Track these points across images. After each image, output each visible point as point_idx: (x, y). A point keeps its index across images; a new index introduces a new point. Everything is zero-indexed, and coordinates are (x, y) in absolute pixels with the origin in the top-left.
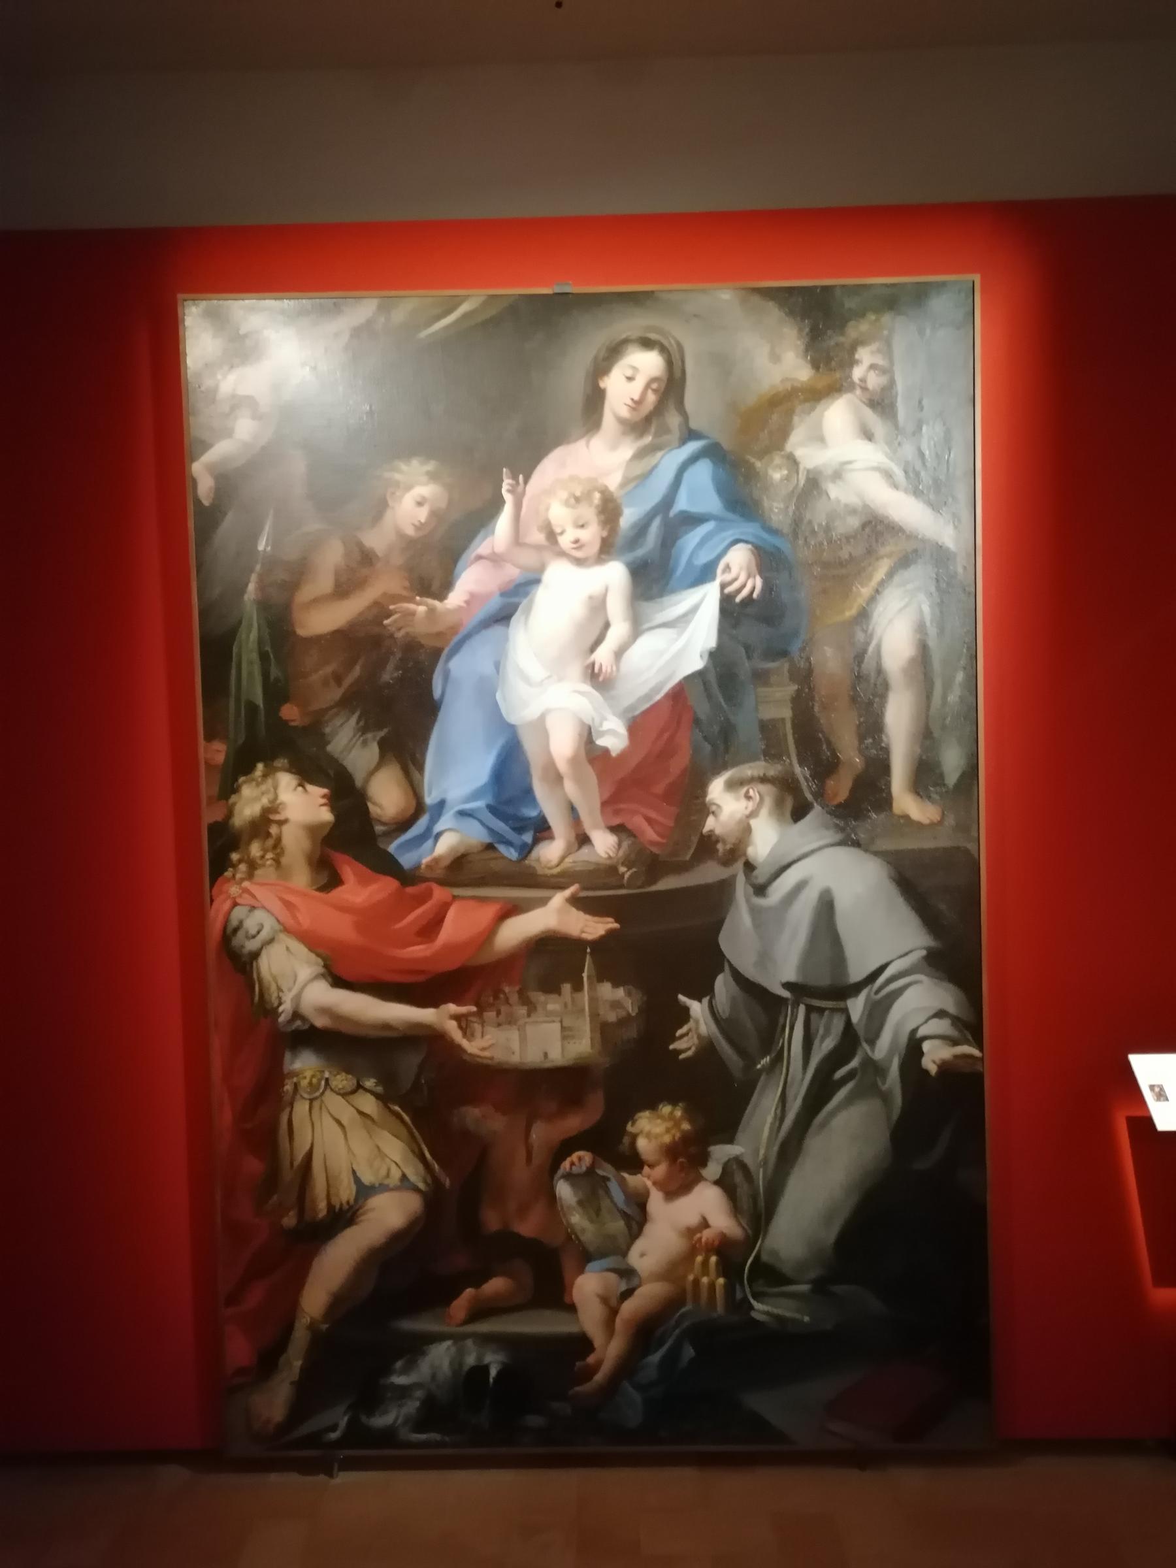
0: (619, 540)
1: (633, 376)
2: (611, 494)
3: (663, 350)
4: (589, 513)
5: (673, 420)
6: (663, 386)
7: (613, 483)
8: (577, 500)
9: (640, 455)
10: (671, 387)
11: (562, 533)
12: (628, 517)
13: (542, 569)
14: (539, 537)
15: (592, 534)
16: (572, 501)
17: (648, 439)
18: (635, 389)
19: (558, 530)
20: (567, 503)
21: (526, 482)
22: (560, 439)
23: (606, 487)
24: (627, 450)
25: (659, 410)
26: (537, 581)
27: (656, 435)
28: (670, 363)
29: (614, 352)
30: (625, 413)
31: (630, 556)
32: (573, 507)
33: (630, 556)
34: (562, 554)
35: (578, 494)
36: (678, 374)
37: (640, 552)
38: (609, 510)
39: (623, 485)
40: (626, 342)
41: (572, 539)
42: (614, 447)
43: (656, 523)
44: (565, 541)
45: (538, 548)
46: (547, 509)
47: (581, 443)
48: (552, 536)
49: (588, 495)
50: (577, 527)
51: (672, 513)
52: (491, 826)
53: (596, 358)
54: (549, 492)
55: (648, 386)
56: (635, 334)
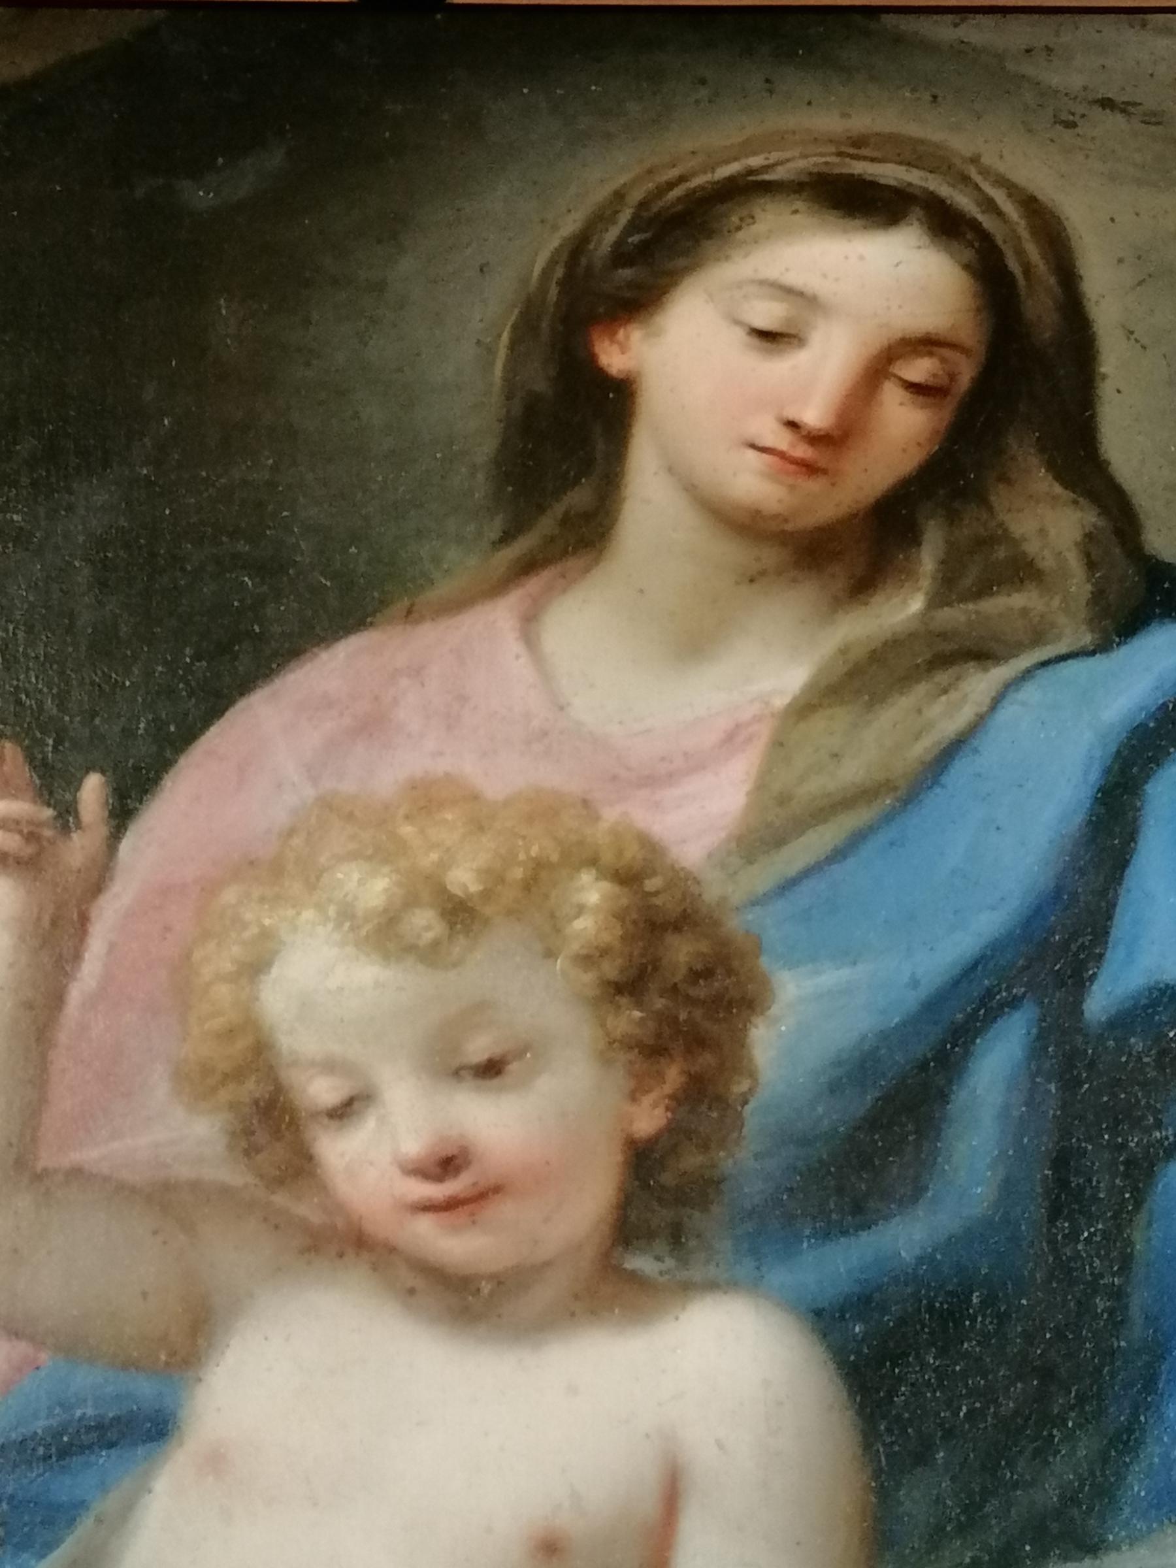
0: (750, 1158)
1: (781, 339)
2: (680, 879)
3: (946, 224)
4: (540, 994)
5: (1048, 522)
6: (966, 373)
7: (698, 820)
8: (460, 914)
9: (861, 681)
10: (1019, 377)
11: (344, 1112)
12: (804, 1025)
13: (190, 1337)
14: (187, 1136)
15: (557, 1119)
16: (424, 923)
17: (902, 608)
18: (815, 381)
19: (323, 1091)
20: (384, 936)
21: (122, 813)
22: (349, 602)
23: (651, 847)
24: (774, 661)
25: (951, 477)
26: (144, 1429)
27: (948, 588)
28: (992, 277)
29: (672, 236)
30: (750, 482)
31: (839, 1263)
32: (431, 955)
33: (839, 1263)
34: (347, 1244)
35: (463, 878)
36: (1040, 308)
37: (905, 1238)
38: (675, 982)
39: (758, 838)
40: (746, 189)
41: (413, 1146)
42: (694, 642)
43: (999, 1061)
44: (368, 1163)
45: (166, 1200)
46: (255, 967)
47: (500, 617)
48: (274, 1124)
49: (532, 890)
50: (447, 1077)
51: (1102, 1000)
52: (103, 831)
53: (578, 246)
54: (280, 868)
55: (878, 369)
56: (793, 163)
